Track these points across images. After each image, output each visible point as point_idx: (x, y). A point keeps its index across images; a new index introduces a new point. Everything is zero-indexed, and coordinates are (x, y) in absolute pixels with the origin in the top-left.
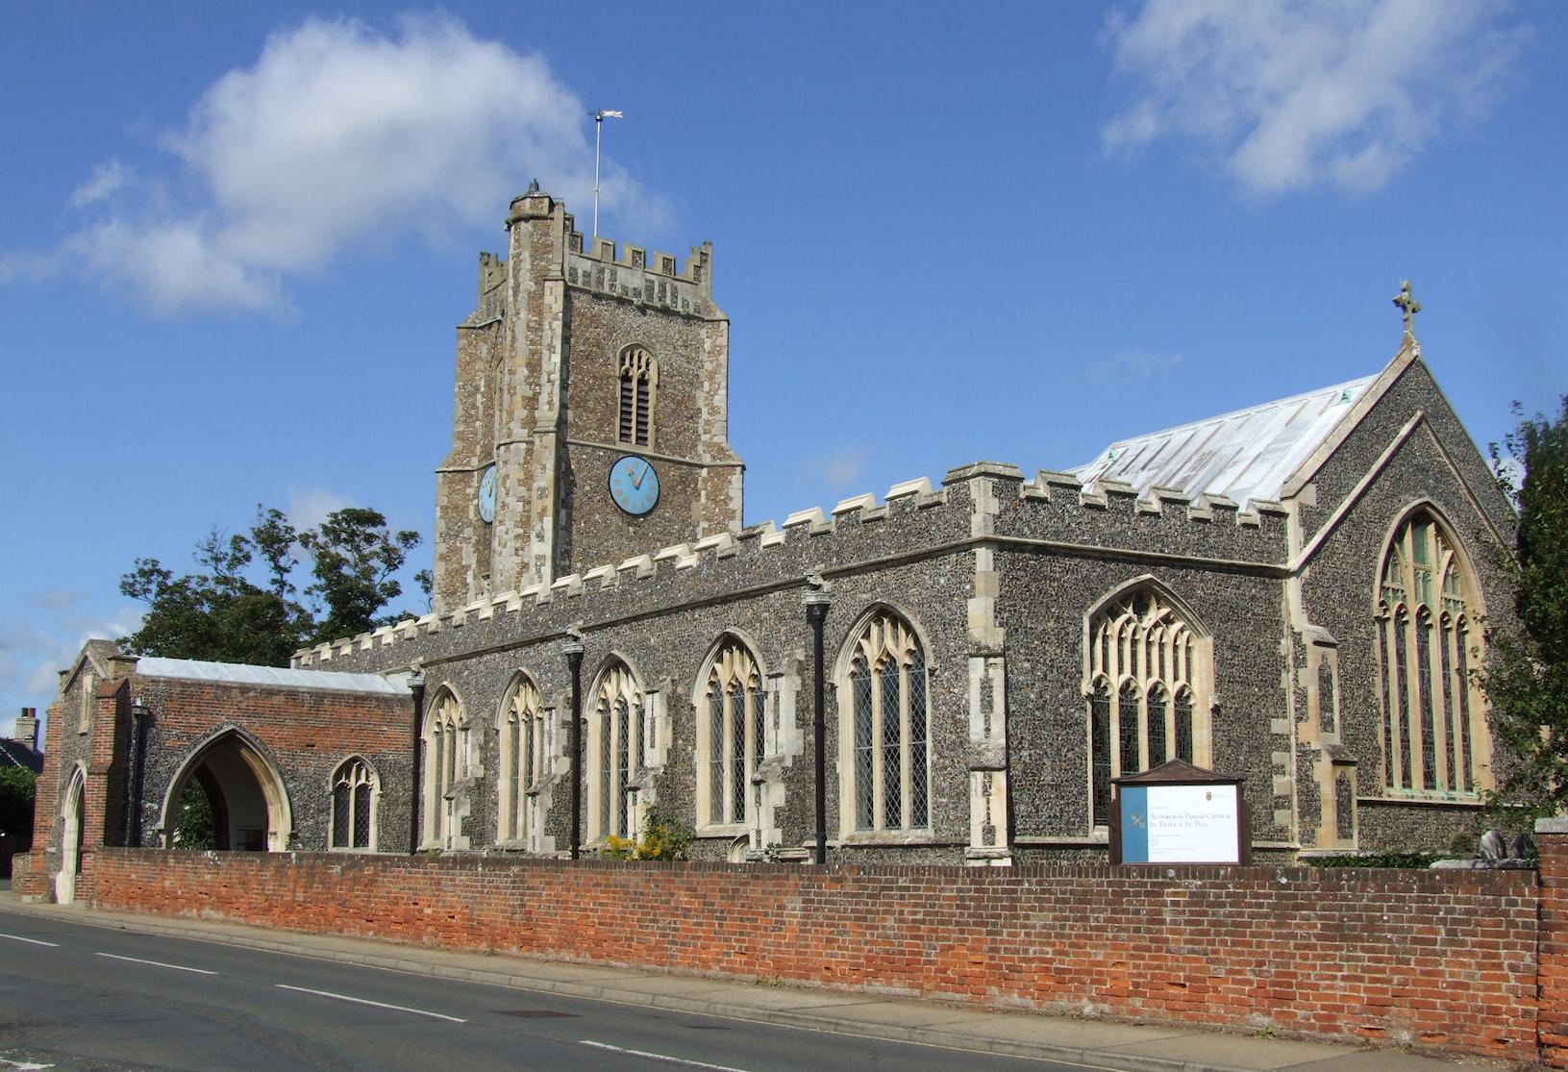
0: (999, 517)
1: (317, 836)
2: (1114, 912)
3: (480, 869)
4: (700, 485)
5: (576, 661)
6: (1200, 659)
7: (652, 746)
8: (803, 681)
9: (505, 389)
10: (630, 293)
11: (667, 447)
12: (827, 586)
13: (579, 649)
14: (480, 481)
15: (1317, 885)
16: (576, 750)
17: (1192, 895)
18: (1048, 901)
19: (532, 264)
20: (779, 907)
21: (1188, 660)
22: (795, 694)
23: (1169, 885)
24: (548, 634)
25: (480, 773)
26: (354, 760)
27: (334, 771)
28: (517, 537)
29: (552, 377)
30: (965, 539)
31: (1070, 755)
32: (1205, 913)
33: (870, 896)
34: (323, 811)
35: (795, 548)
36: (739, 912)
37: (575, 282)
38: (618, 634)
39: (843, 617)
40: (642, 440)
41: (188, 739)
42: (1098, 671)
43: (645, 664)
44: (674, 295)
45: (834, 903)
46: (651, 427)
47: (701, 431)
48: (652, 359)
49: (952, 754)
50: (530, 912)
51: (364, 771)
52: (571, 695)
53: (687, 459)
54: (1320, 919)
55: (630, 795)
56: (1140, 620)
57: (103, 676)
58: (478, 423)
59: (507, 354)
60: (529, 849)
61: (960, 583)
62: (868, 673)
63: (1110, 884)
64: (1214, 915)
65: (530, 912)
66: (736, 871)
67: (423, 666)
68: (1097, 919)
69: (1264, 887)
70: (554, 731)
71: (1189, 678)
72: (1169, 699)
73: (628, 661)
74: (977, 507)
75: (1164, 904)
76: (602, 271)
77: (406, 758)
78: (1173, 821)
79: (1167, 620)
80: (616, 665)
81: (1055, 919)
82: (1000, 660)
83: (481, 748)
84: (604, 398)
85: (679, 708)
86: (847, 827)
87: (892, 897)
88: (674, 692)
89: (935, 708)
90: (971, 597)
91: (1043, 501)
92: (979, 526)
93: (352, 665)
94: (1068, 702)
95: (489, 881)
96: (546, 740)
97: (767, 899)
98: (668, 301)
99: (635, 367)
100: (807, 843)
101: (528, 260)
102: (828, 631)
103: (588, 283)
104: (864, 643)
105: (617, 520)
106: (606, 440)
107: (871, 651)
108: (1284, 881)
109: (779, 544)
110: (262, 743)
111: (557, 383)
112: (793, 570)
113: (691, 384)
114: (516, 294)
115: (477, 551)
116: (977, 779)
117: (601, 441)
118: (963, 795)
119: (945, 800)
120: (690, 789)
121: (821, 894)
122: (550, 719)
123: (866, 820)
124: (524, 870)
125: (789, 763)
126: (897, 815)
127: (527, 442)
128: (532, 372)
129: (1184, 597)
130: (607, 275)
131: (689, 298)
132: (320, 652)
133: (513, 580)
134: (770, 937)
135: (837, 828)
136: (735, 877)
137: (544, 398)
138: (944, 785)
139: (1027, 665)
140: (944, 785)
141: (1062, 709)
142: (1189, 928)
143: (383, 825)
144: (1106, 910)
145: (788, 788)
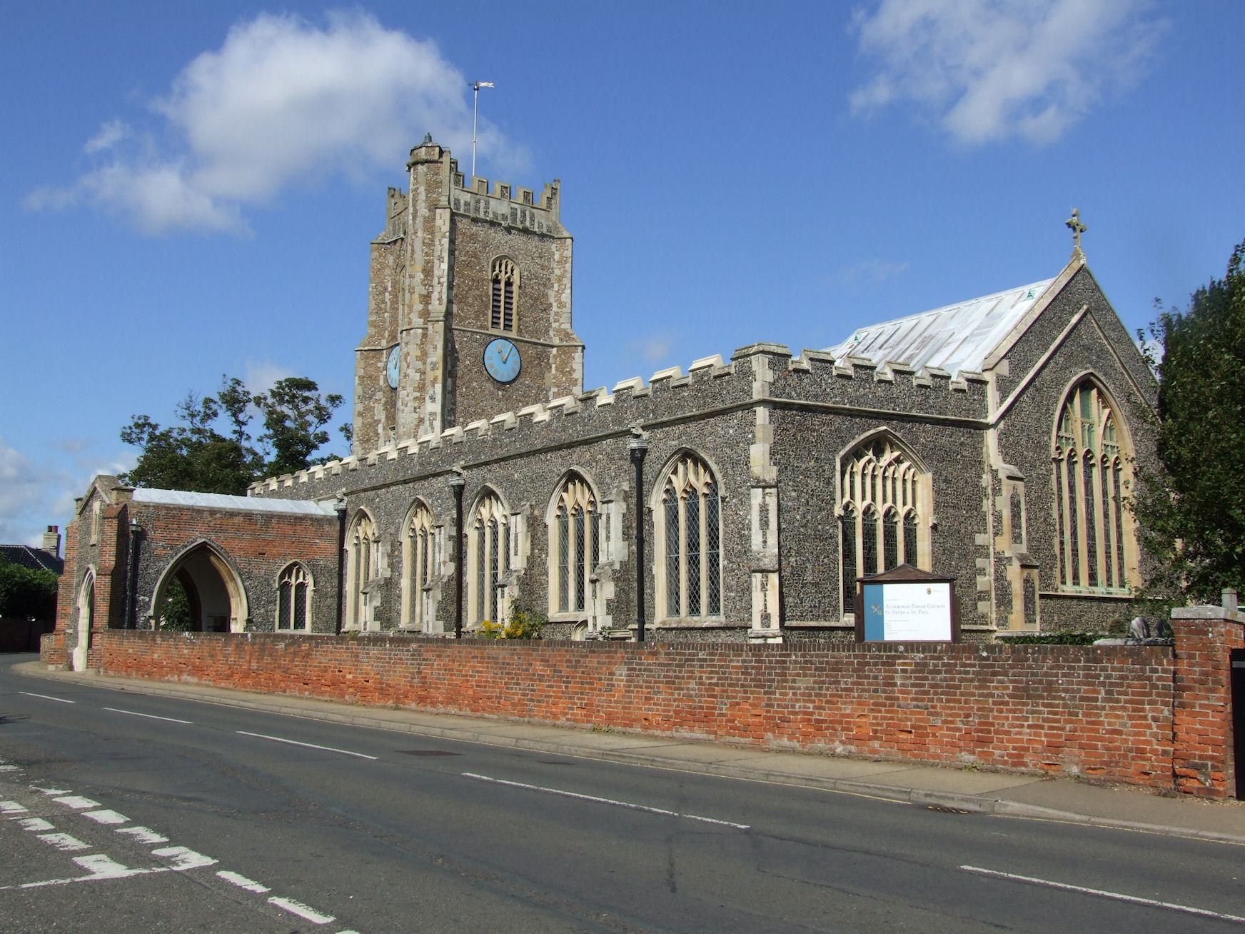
0: (773, 384)
1: (267, 616)
2: (858, 677)
3: (388, 645)
4: (551, 361)
5: (459, 491)
6: (923, 490)
7: (516, 554)
9: (407, 289)
11: (527, 332)
12: (646, 435)
13: (462, 482)
14: (388, 357)
16: (459, 557)
17: (917, 664)
18: (810, 669)
19: (427, 197)
20: (610, 674)
21: (914, 490)
22: (621, 516)
23: (899, 658)
24: (438, 471)
25: (388, 574)
26: (295, 564)
27: (279, 573)
28: (416, 399)
29: (441, 280)
30: (748, 401)
31: (826, 561)
32: (927, 678)
34: (271, 602)
35: (622, 407)
36: (581, 677)
37: (458, 209)
38: (490, 471)
39: (658, 458)
40: (508, 327)
41: (171, 549)
42: (847, 498)
43: (510, 493)
44: (532, 219)
45: (651, 671)
46: (515, 317)
47: (552, 320)
49: (738, 560)
51: (301, 573)
52: (455, 516)
54: (1011, 683)
55: (499, 590)
56: (878, 460)
57: (108, 502)
58: (386, 314)
60: (424, 631)
61: (745, 433)
62: (676, 500)
63: (856, 656)
64: (933, 679)
65: (425, 677)
67: (345, 495)
68: (846, 683)
69: (970, 659)
70: (443, 543)
71: (914, 504)
72: (900, 520)
73: (498, 491)
75: (896, 671)
76: (478, 201)
77: (333, 563)
79: (898, 461)
80: (489, 494)
81: (815, 682)
82: (774, 490)
83: (389, 556)
84: (480, 296)
85: (535, 526)
86: (660, 614)
87: (694, 666)
88: (532, 513)
89: (726, 526)
90: (752, 443)
91: (806, 372)
92: (758, 391)
93: (293, 494)
95: (395, 655)
96: (437, 549)
98: (528, 224)
100: (630, 626)
101: (424, 193)
102: (646, 469)
103: (469, 210)
104: (673, 477)
105: (489, 386)
106: (481, 327)
107: (678, 483)
108: (985, 654)
110: (226, 552)
111: (445, 284)
112: (620, 423)
113: (545, 285)
115: (386, 409)
116: (757, 579)
117: (478, 328)
119: (733, 594)
120: (544, 586)
122: (440, 534)
123: (674, 609)
124: (420, 646)
126: (697, 606)
127: (423, 329)
128: (426, 276)
130: (482, 204)
131: (543, 221)
135: (653, 615)
137: (435, 296)
138: (732, 583)
139: (794, 494)
141: (820, 527)
142: (914, 689)
143: (316, 613)
145: (616, 586)
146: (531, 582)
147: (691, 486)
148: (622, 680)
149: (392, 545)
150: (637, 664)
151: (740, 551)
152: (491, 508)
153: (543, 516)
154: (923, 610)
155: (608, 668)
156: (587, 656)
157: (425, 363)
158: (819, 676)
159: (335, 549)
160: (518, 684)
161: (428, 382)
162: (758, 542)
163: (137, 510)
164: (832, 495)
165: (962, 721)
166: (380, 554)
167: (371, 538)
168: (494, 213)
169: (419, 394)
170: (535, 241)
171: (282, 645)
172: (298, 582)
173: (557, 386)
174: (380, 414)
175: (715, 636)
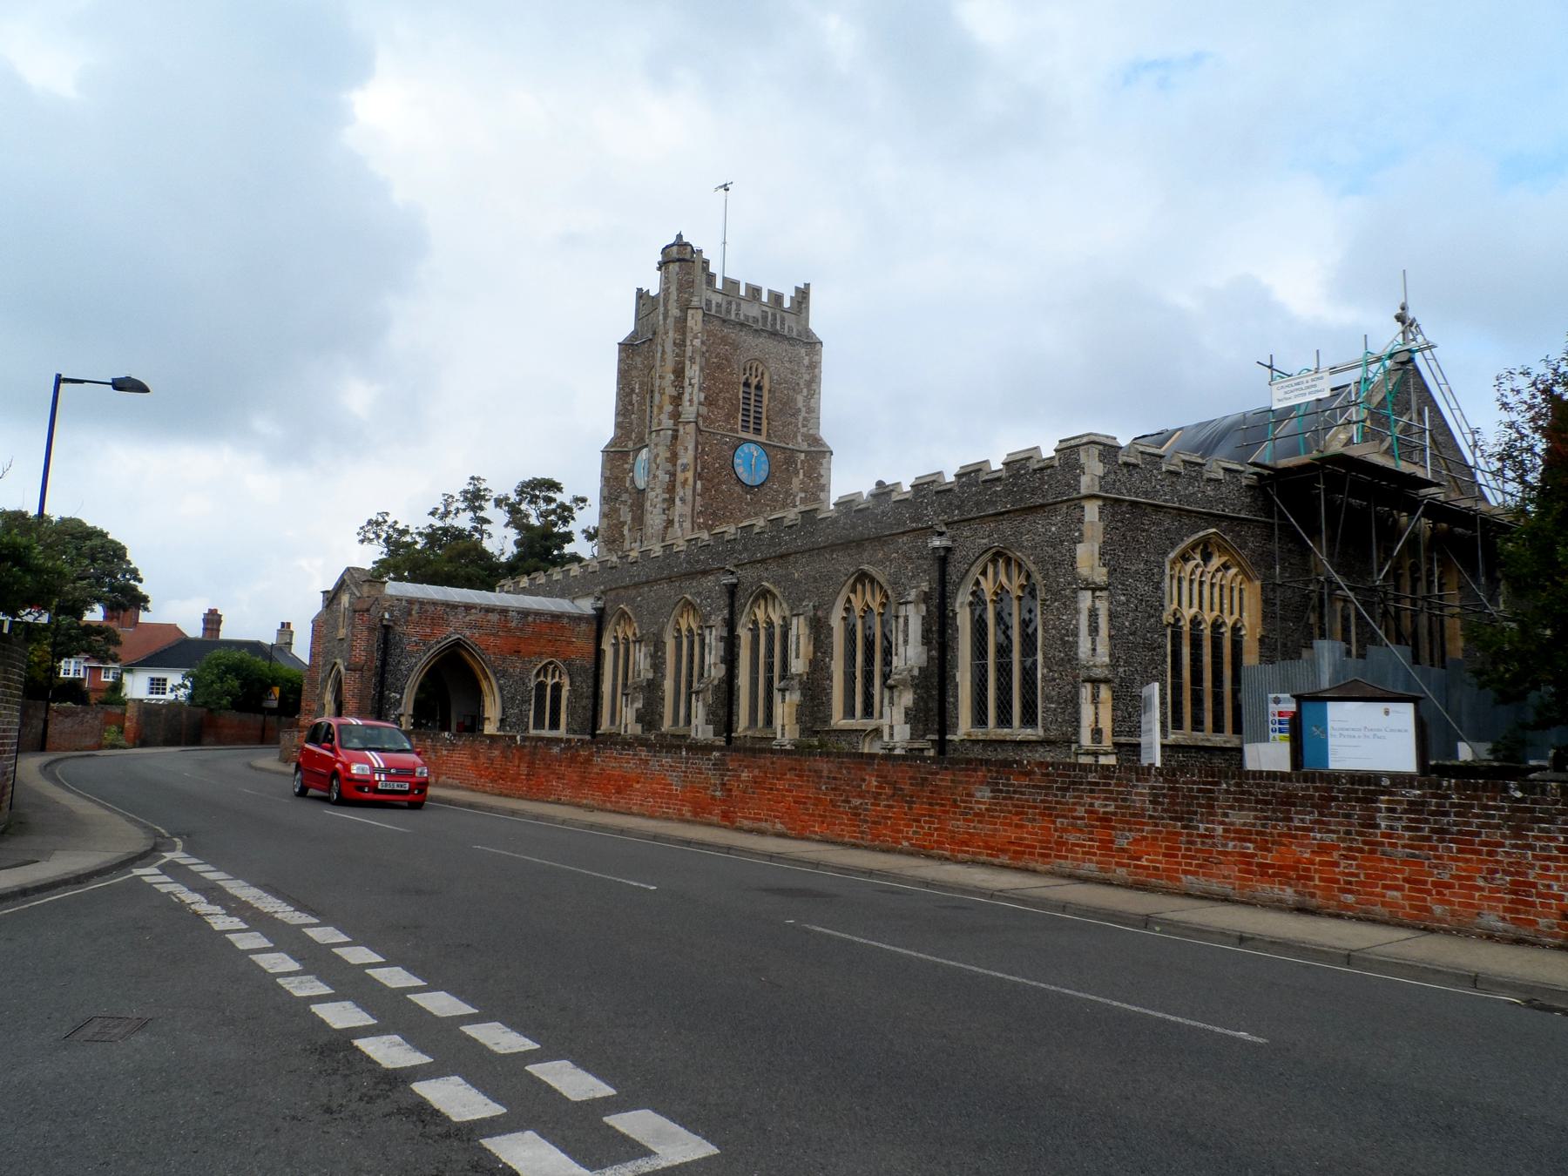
0: (1103, 478)
1: (523, 715)
2: (1321, 814)
3: (684, 753)
4: (799, 466)
5: (732, 590)
6: (1250, 598)
7: (797, 656)
8: (928, 608)
9: (657, 389)
10: (750, 320)
11: (776, 436)
12: (949, 533)
13: (735, 581)
14: (635, 459)
15: (1559, 801)
16: (730, 659)
17: (1410, 803)
18: (1249, 801)
19: (678, 296)
20: (968, 795)
21: (1241, 599)
22: (920, 618)
23: (1383, 793)
24: (708, 568)
25: (650, 676)
26: (551, 663)
27: (535, 672)
28: (664, 500)
29: (693, 381)
30: (1075, 495)
31: (1154, 672)
32: (1426, 821)
33: (1058, 789)
34: (526, 702)
35: (922, 502)
36: (928, 798)
37: (709, 310)
38: (767, 569)
39: (964, 557)
40: (758, 431)
41: (424, 645)
42: (1175, 605)
43: (790, 593)
44: (783, 323)
45: (1022, 793)
46: (764, 422)
47: (800, 425)
48: (765, 371)
49: (1061, 668)
50: (730, 790)
51: (557, 673)
52: (727, 616)
53: (790, 446)
54: (1561, 833)
55: (694, 696)
56: (1205, 565)
57: (358, 595)
58: (633, 416)
59: (658, 363)
60: (693, 734)
61: (1071, 530)
62: (985, 603)
63: (1316, 789)
64: (1436, 822)
65: (730, 790)
66: (926, 762)
67: (603, 592)
68: (1302, 821)
69: (1494, 799)
70: (714, 644)
71: (1241, 615)
72: (1227, 632)
73: (776, 591)
74: (1086, 471)
75: (1379, 810)
76: (730, 303)
77: (589, 663)
78: (1352, 733)
79: (1226, 567)
80: (765, 595)
81: (1256, 818)
82: (1104, 594)
83: (651, 656)
84: (730, 399)
85: (819, 629)
86: (964, 725)
87: (1082, 791)
88: (815, 614)
89: (1045, 631)
90: (1080, 542)
91: (1135, 466)
92: (1087, 484)
93: (548, 592)
94: (1153, 630)
95: (692, 763)
96: (707, 650)
97: (956, 788)
98: (778, 327)
99: (754, 376)
100: (928, 737)
101: (675, 293)
102: (951, 569)
103: (720, 312)
104: (981, 579)
105: (738, 489)
106: (732, 430)
107: (988, 586)
108: (1519, 794)
109: (907, 499)
110: (480, 648)
111: (696, 386)
112: (919, 520)
113: (794, 390)
114: (665, 318)
115: (632, 511)
116: (1086, 692)
117: (728, 431)
118: (1074, 702)
119: (1053, 706)
120: (828, 694)
121: (1008, 785)
122: (711, 634)
123: (980, 718)
124: (724, 755)
125: (916, 672)
126: (1008, 717)
127: (673, 430)
128: (677, 377)
129: (1240, 547)
130: (734, 307)
131: (793, 325)
132: (570, 570)
133: (661, 532)
134: (959, 820)
135: (956, 725)
136: (924, 767)
137: (686, 397)
138: (1053, 693)
139: (1123, 598)
140: (1053, 693)
141: (1149, 635)
142: (1407, 834)
143: (571, 714)
144: (1313, 813)
145: (915, 693)
146: (814, 691)
147: (868, 606)
148: (984, 803)
149: (655, 646)
150: (1003, 785)
151: (1062, 659)
152: (996, 574)
153: (827, 617)
154: (1379, 734)
155: (965, 789)
156: (937, 773)
157: (675, 465)
158: (1262, 810)
159: (591, 647)
160: (848, 802)
161: (678, 484)
162: (1084, 650)
163: (389, 603)
164: (1161, 600)
165: (1483, 877)
166: (642, 654)
167: (631, 638)
168: (745, 315)
169: (667, 496)
170: (785, 345)
171: (556, 750)
172: (554, 681)
173: (806, 492)
174: (626, 515)
175: (1030, 751)
